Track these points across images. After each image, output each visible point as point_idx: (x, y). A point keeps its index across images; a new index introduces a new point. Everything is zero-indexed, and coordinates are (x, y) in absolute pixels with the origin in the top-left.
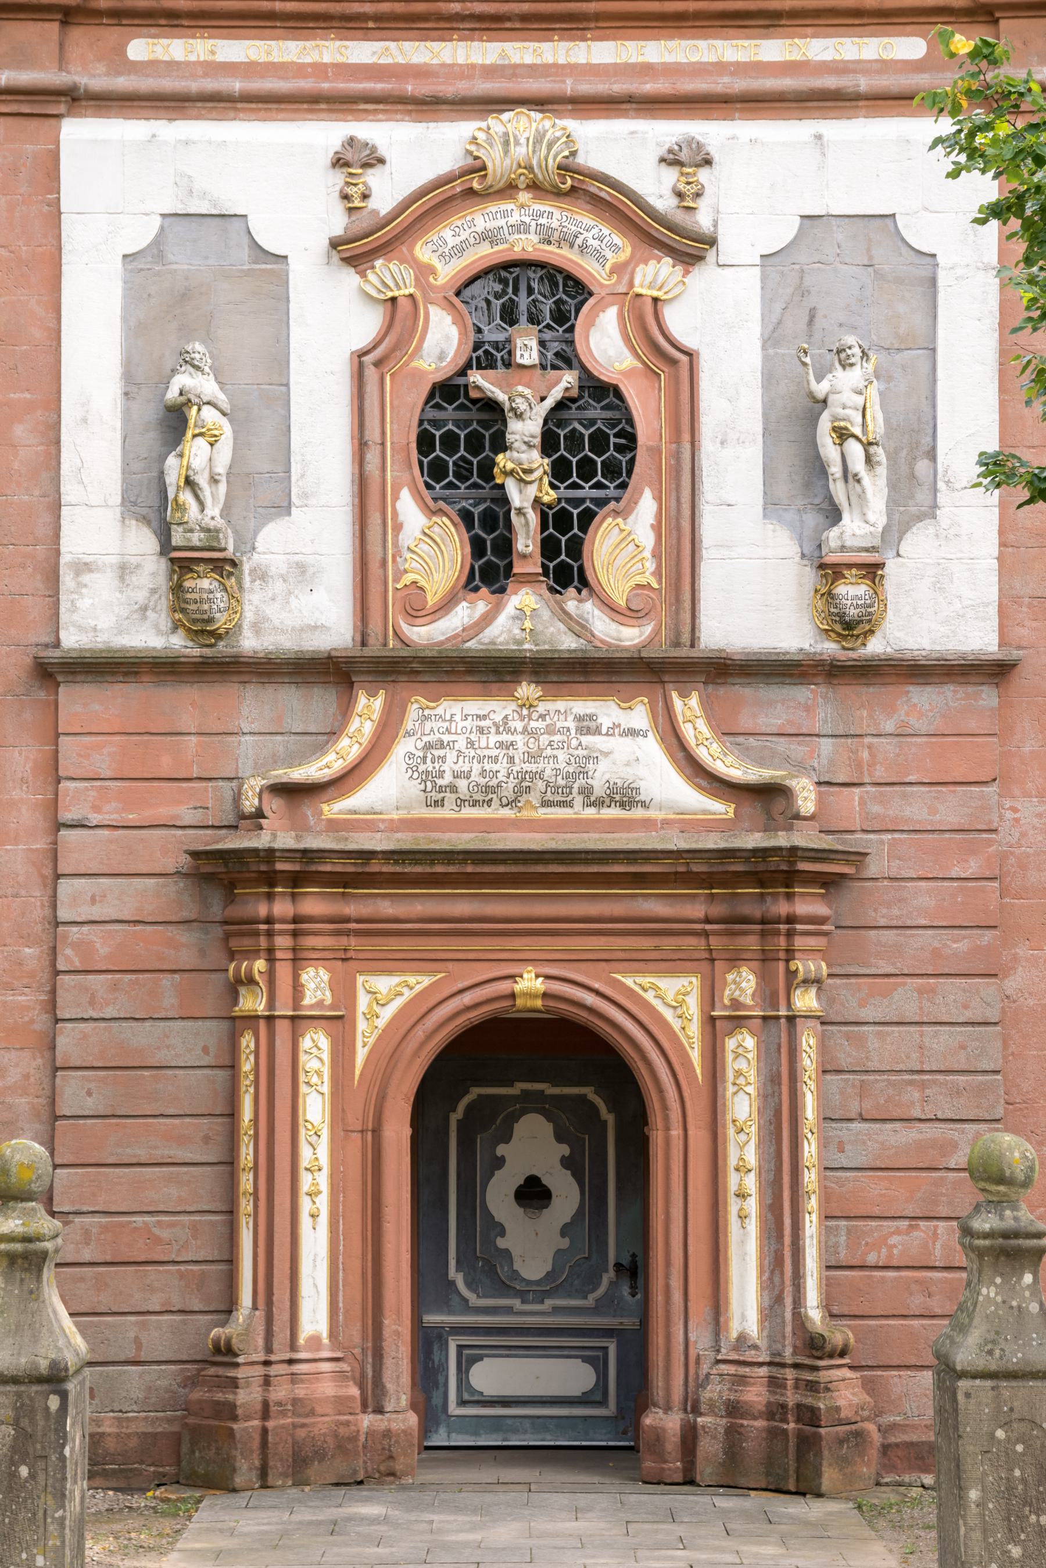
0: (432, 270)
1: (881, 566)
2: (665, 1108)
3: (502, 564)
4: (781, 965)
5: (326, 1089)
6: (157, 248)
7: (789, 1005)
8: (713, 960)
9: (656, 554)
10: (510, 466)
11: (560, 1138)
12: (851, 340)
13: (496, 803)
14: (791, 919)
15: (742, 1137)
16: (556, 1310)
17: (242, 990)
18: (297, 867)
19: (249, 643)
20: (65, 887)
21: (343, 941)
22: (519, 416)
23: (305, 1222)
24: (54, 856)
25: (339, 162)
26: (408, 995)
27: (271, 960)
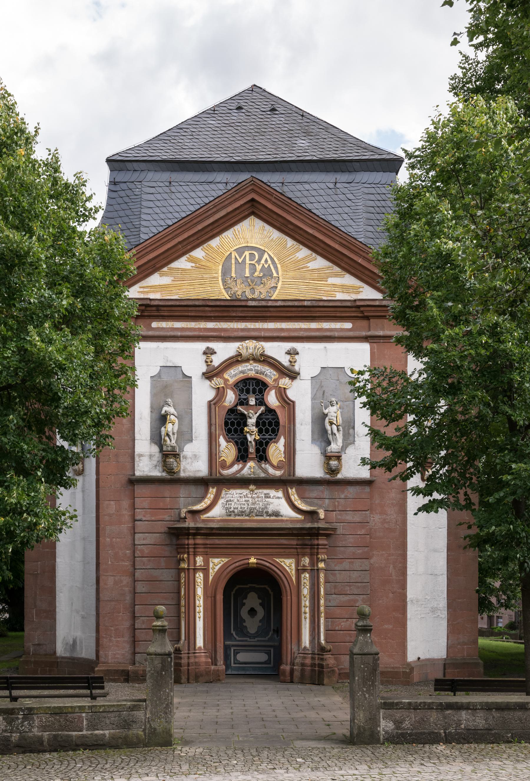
1: (341, 456)
4: (315, 556)
5: (202, 586)
6: (159, 375)
8: (298, 555)
9: (285, 452)
10: (248, 430)
12: (333, 399)
14: (318, 545)
15: (305, 599)
16: (258, 641)
17: (181, 562)
19: (182, 475)
20: (137, 536)
21: (206, 550)
22: (250, 418)
23: (197, 619)
25: (205, 353)
26: (222, 563)
27: (188, 555)
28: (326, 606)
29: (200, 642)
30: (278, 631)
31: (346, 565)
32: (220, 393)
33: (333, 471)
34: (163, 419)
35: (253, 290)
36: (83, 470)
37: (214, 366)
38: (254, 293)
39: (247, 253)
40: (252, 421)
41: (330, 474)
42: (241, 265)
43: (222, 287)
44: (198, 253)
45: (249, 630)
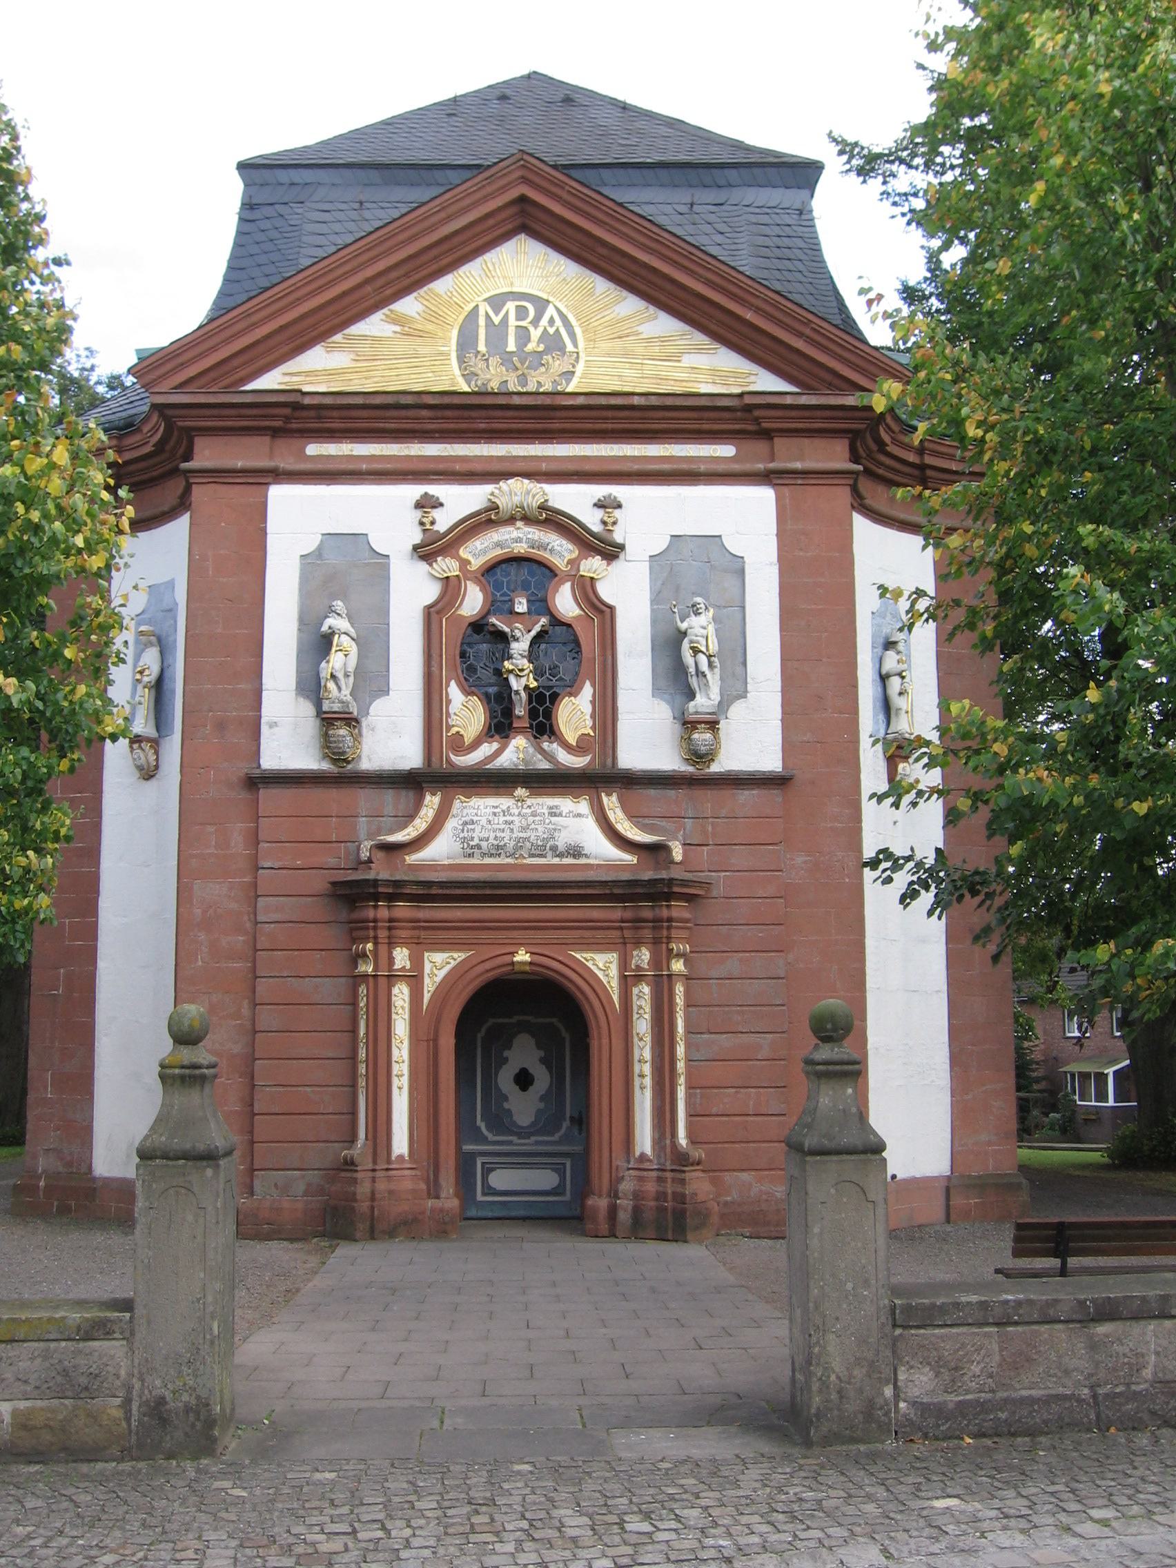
0: (469, 563)
1: (717, 723)
2: (599, 1027)
3: (507, 722)
4: (664, 946)
5: (407, 1016)
6: (319, 552)
7: (668, 969)
8: (625, 943)
9: (593, 716)
10: (511, 667)
11: (539, 1047)
12: (699, 600)
13: (503, 855)
14: (670, 920)
15: (641, 1044)
16: (537, 1143)
17: (360, 961)
18: (390, 891)
19: (365, 765)
20: (262, 902)
21: (416, 933)
22: (517, 640)
23: (395, 1091)
24: (255, 885)
25: (419, 505)
26: (453, 963)
27: (376, 944)
28: (689, 1060)
29: (400, 1144)
30: (581, 1121)
31: (733, 965)
32: (451, 589)
33: (699, 757)
34: (323, 644)
35: (523, 379)
36: (157, 767)
37: (438, 532)
38: (525, 385)
39: (511, 306)
40: (520, 646)
41: (694, 764)
42: (497, 332)
43: (457, 372)
44: (408, 306)
45: (515, 1118)
